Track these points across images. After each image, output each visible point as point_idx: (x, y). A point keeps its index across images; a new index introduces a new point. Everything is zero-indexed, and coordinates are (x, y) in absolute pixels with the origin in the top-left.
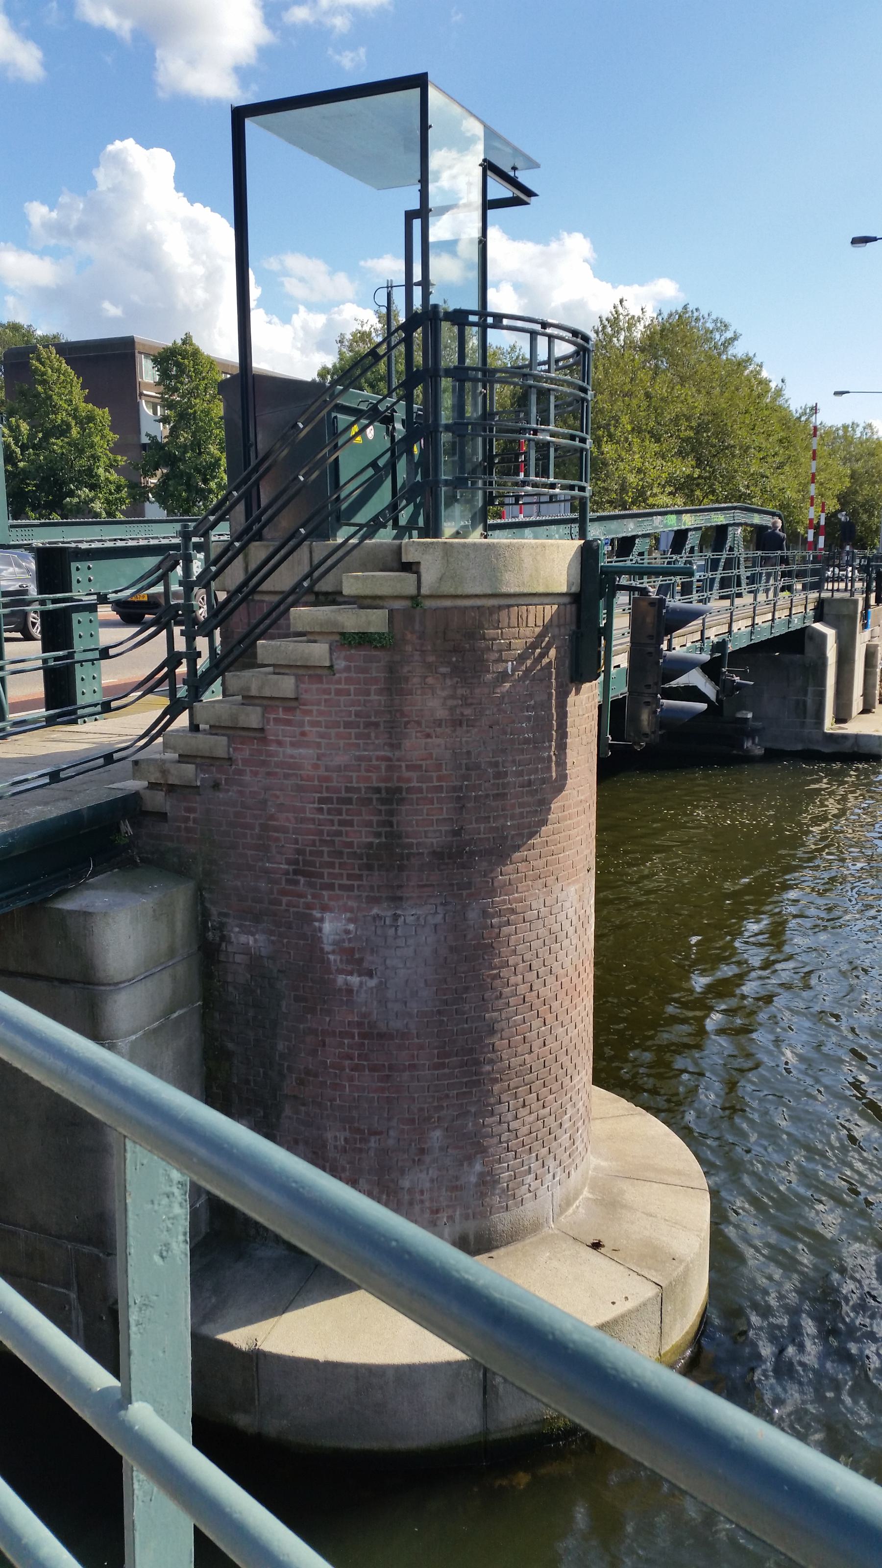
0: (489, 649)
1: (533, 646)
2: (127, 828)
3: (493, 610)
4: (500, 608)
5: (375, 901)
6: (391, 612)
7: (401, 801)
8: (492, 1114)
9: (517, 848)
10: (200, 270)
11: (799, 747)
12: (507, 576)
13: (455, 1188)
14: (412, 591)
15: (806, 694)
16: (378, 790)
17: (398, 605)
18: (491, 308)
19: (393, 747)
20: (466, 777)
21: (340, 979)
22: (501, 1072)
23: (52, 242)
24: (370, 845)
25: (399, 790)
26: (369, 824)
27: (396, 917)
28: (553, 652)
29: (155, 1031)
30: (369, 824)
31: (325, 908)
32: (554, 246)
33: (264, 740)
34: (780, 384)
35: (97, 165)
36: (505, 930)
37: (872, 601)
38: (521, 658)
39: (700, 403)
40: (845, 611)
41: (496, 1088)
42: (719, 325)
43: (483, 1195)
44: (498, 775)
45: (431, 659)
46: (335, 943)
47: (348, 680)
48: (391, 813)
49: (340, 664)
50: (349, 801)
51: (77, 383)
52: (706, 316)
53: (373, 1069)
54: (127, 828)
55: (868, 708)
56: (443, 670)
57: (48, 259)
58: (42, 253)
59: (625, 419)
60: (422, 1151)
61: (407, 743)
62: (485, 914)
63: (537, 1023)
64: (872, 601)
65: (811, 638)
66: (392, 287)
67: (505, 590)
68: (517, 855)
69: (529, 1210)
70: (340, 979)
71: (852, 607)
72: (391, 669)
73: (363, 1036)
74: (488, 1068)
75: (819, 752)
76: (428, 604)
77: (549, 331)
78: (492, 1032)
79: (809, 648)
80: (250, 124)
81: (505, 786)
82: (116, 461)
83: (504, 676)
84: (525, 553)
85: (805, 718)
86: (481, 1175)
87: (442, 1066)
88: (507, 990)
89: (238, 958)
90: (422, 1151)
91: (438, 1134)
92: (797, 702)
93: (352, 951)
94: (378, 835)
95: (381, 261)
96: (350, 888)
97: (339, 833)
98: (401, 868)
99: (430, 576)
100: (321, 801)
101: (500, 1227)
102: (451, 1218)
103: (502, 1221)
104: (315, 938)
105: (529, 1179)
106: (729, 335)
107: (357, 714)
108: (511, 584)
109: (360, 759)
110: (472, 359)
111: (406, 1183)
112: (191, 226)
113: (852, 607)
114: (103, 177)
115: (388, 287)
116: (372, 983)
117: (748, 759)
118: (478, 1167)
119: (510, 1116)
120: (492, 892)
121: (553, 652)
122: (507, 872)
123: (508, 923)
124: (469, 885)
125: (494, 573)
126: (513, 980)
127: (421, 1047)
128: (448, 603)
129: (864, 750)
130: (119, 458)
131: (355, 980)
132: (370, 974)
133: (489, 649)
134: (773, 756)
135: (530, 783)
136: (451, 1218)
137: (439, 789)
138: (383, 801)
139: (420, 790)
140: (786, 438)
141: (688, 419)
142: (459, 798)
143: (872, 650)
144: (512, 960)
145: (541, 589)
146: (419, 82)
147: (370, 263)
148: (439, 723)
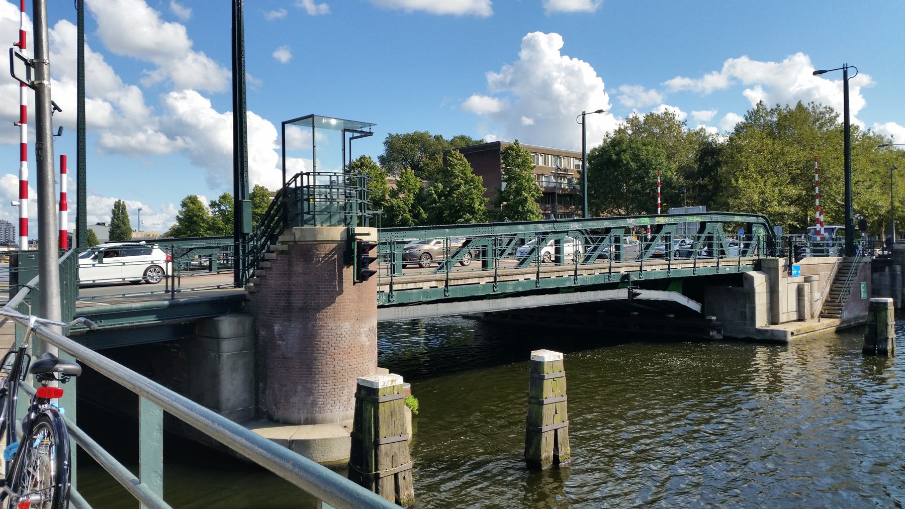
0: (314, 255)
1: (328, 254)
2: (243, 304)
3: (315, 245)
4: (317, 244)
5: (285, 321)
6: (289, 245)
7: (291, 294)
8: (316, 384)
9: (324, 309)
10: (574, 97)
11: (744, 336)
12: (319, 236)
13: (304, 403)
14: (293, 240)
15: (745, 308)
16: (286, 291)
17: (292, 243)
18: (317, 170)
19: (289, 280)
20: (308, 288)
21: (278, 342)
22: (319, 372)
23: (498, 91)
24: (284, 306)
25: (291, 291)
26: (284, 300)
27: (290, 325)
28: (336, 256)
29: (237, 354)
30: (284, 300)
31: (275, 323)
32: (786, 62)
33: (266, 279)
34: (890, 138)
35: (520, 50)
36: (320, 331)
37: (793, 261)
38: (324, 257)
39: (804, 155)
40: (772, 265)
41: (317, 376)
42: (828, 109)
43: (313, 407)
44: (317, 288)
45: (298, 257)
46: (277, 332)
47: (280, 263)
48: (289, 297)
49: (279, 258)
50: (279, 294)
51: (469, 165)
52: (818, 105)
53: (285, 367)
54: (243, 304)
55: (802, 318)
56: (302, 260)
57: (496, 99)
58: (494, 96)
59: (751, 166)
60: (296, 392)
61: (293, 279)
62: (313, 326)
63: (331, 360)
64: (793, 261)
65: (746, 279)
66: (847, 68)
67: (318, 239)
68: (323, 311)
69: (328, 415)
70: (278, 342)
71: (775, 263)
72: (289, 260)
73: (282, 358)
74: (314, 370)
75: (754, 339)
76: (299, 243)
77: (337, 174)
78: (316, 360)
79: (745, 284)
80: (286, 125)
81: (319, 291)
82: (484, 200)
83: (319, 262)
84: (324, 230)
85: (746, 320)
86: (312, 401)
87: (301, 368)
88: (320, 349)
89: (261, 338)
90: (296, 392)
91: (300, 387)
92: (742, 312)
93: (280, 334)
94: (286, 303)
95: (673, 80)
96: (279, 317)
97: (278, 303)
98: (291, 312)
99: (297, 236)
100: (276, 294)
101: (318, 418)
102: (303, 412)
103: (319, 416)
104: (273, 331)
105: (329, 405)
106: (833, 114)
107: (282, 271)
108: (320, 238)
109: (283, 283)
110: (311, 183)
111: (291, 400)
112: (571, 72)
113: (775, 263)
114: (524, 54)
115: (844, 68)
116: (284, 343)
117: (711, 340)
118: (311, 399)
119: (322, 385)
120: (315, 320)
121: (336, 256)
122: (320, 315)
123: (321, 329)
124: (308, 318)
125: (315, 235)
126: (322, 346)
127: (295, 362)
128: (303, 243)
129: (777, 338)
130: (485, 199)
131: (281, 342)
132: (284, 341)
133: (314, 255)
134: (727, 340)
135: (328, 291)
136: (303, 412)
137: (300, 291)
138: (287, 294)
139: (296, 291)
140: (876, 171)
141: (797, 163)
142: (306, 294)
143: (801, 287)
144: (322, 340)
145: (330, 239)
146: (312, 116)
147: (669, 82)
148: (300, 274)
